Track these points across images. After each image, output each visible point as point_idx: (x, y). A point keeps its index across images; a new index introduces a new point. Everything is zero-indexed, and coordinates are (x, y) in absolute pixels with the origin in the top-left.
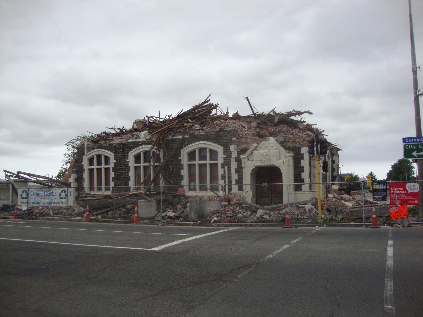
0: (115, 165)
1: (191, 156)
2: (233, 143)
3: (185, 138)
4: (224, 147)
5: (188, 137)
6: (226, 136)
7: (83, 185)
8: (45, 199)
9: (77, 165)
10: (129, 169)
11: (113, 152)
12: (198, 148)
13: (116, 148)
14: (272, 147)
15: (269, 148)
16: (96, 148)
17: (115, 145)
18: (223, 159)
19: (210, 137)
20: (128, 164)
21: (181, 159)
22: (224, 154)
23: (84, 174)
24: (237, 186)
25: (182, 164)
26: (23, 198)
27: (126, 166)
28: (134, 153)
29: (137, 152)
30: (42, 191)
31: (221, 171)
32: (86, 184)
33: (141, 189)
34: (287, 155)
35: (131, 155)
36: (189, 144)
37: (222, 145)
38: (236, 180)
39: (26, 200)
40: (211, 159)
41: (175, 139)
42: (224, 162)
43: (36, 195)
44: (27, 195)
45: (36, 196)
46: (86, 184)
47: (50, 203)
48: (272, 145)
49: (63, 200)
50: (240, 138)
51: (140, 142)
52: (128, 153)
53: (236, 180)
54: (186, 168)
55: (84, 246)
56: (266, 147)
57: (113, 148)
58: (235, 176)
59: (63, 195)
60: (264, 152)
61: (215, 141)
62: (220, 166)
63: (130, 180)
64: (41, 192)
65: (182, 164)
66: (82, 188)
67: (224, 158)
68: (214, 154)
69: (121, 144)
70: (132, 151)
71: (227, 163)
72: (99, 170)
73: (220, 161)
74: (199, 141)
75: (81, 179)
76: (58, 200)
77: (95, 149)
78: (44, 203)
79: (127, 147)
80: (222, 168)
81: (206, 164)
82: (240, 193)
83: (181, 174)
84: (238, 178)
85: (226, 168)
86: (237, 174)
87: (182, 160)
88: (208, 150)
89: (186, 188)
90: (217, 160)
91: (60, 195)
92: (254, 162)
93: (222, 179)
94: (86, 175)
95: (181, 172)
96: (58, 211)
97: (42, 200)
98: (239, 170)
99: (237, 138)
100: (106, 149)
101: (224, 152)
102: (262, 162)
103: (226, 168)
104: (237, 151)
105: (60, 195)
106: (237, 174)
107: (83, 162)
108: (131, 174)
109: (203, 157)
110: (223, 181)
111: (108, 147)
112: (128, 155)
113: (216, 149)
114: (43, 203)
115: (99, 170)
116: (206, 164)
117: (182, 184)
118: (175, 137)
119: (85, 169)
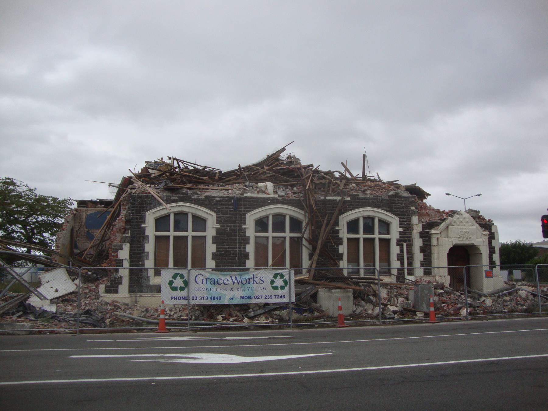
0: (217, 233)
1: (353, 226)
2: (413, 213)
3: (345, 201)
4: (400, 218)
5: (349, 199)
6: (402, 203)
7: (143, 265)
8: (232, 290)
9: (128, 227)
10: (246, 240)
11: (215, 212)
12: (173, 212)
13: (223, 204)
14: (467, 222)
15: (458, 223)
16: (177, 201)
17: (218, 199)
18: (399, 233)
19: (381, 202)
20: (245, 232)
21: (338, 230)
22: (400, 227)
23: (146, 245)
24: (423, 269)
25: (340, 236)
26: (174, 289)
27: (241, 236)
28: (258, 216)
29: (263, 214)
30: (222, 275)
31: (395, 250)
32: (149, 263)
33: (301, 273)
34: (484, 233)
35: (251, 217)
36: (351, 210)
37: (397, 215)
38: (421, 262)
39: (184, 293)
40: (365, 232)
41: (329, 200)
42: (400, 237)
43: (208, 283)
44: (186, 283)
45: (209, 286)
46: (149, 263)
47: (250, 298)
48: (467, 220)
49: (280, 292)
50: (419, 208)
51: (269, 198)
52: (245, 214)
53: (421, 262)
54: (152, 240)
55: (200, 375)
56: (461, 222)
57: (215, 204)
58: (418, 257)
59: (179, 282)
60: (463, 228)
61: (389, 209)
62: (209, 240)
63: (248, 259)
64: (223, 278)
65: (340, 236)
66: (141, 270)
67: (400, 232)
68: (385, 226)
69: (230, 198)
70: (253, 212)
71: (405, 238)
72: (369, 242)
73: (395, 234)
74: (366, 206)
75: (139, 254)
76: (269, 291)
77: (173, 201)
78: (230, 299)
79: (244, 205)
80: (398, 245)
81: (186, 237)
82: (427, 278)
83: (338, 251)
84: (424, 259)
85: (405, 246)
86: (422, 254)
87: (340, 231)
88: (377, 221)
89: (151, 273)
90: (205, 231)
91: (272, 282)
92: (451, 240)
93: (398, 260)
94: (150, 247)
95: (338, 249)
96: (268, 309)
97: (224, 292)
98: (426, 249)
99: (416, 208)
100: (200, 205)
101: (400, 224)
102: (461, 239)
103: (405, 246)
104: (423, 225)
105: (272, 282)
106: (422, 254)
107: (245, 224)
108: (343, 249)
109: (369, 229)
110: (399, 262)
111: (203, 200)
112: (245, 218)
113: (204, 215)
114: (227, 298)
115: (369, 242)
116: (186, 237)
117: (341, 267)
118: (328, 198)
119: (148, 237)
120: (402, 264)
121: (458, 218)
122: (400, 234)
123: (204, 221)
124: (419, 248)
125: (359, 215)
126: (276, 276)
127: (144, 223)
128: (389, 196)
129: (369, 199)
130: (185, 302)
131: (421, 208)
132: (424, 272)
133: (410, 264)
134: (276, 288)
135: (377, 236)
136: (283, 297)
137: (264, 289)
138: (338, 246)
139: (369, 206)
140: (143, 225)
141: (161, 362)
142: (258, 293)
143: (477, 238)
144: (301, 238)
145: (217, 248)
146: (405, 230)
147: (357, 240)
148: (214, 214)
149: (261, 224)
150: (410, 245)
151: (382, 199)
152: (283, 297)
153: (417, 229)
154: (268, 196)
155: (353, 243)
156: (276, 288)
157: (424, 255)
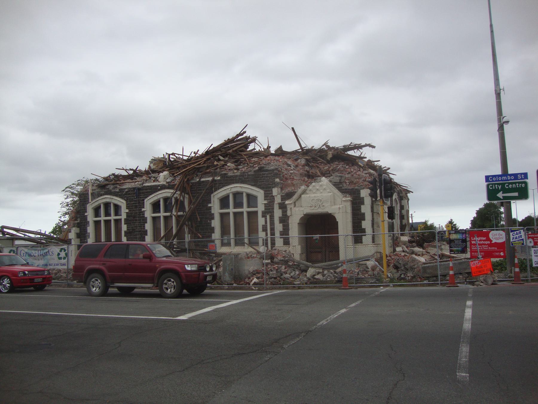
2: (275, 185)
3: (216, 181)
5: (219, 178)
6: (267, 177)
8: (39, 260)
10: (145, 220)
13: (129, 194)
14: (325, 189)
15: (314, 191)
17: (127, 190)
20: (144, 214)
21: (211, 207)
25: (212, 212)
28: (152, 200)
29: (156, 198)
31: (261, 221)
34: (344, 199)
35: (148, 202)
38: (280, 232)
41: (203, 181)
43: (27, 255)
45: (27, 257)
47: (46, 265)
48: (324, 187)
49: (63, 261)
50: (284, 179)
51: (159, 186)
52: (143, 200)
53: (280, 232)
54: (217, 218)
56: (318, 190)
57: (125, 194)
58: (279, 227)
59: (63, 254)
61: (253, 184)
62: (260, 214)
65: (212, 212)
67: (265, 204)
68: (252, 200)
69: (134, 188)
70: (148, 198)
71: (269, 210)
72: (107, 222)
76: (56, 261)
77: (101, 195)
79: (143, 193)
80: (263, 217)
82: (285, 248)
84: (283, 229)
85: (268, 217)
86: (281, 225)
88: (244, 195)
89: (218, 243)
90: (257, 207)
91: (59, 254)
92: (302, 209)
98: (284, 220)
99: (281, 180)
100: (116, 196)
102: (313, 208)
103: (268, 217)
104: (281, 196)
105: (59, 254)
106: (281, 225)
109: (238, 204)
110: (264, 233)
111: (118, 192)
115: (107, 222)
116: (242, 213)
119: (89, 222)
120: (267, 234)
121: (314, 186)
122: (265, 206)
123: (255, 198)
124: (278, 219)
125: (159, 197)
126: (61, 250)
127: (144, 207)
128: (255, 171)
129: (236, 176)
130: (66, 267)
131: (287, 179)
132: (284, 242)
133: (273, 234)
134: (60, 258)
135: (245, 209)
136: (64, 265)
137: (53, 259)
138: (210, 221)
139: (236, 183)
140: (143, 210)
141: (342, 314)
142: (51, 262)
143: (331, 205)
144: (171, 216)
145: (127, 227)
146: (270, 202)
147: (159, 217)
148: (124, 202)
149: (156, 206)
150: (272, 217)
151: (248, 175)
152: (64, 265)
153: (278, 200)
154: (159, 183)
155: (224, 217)
156: (60, 258)
157: (284, 226)
